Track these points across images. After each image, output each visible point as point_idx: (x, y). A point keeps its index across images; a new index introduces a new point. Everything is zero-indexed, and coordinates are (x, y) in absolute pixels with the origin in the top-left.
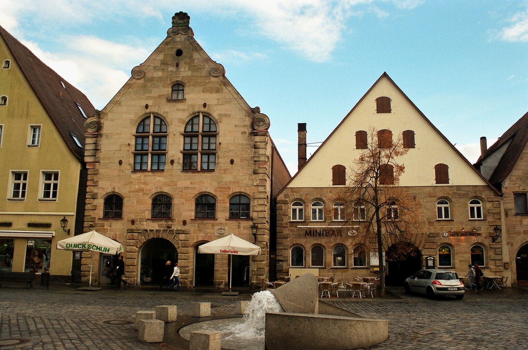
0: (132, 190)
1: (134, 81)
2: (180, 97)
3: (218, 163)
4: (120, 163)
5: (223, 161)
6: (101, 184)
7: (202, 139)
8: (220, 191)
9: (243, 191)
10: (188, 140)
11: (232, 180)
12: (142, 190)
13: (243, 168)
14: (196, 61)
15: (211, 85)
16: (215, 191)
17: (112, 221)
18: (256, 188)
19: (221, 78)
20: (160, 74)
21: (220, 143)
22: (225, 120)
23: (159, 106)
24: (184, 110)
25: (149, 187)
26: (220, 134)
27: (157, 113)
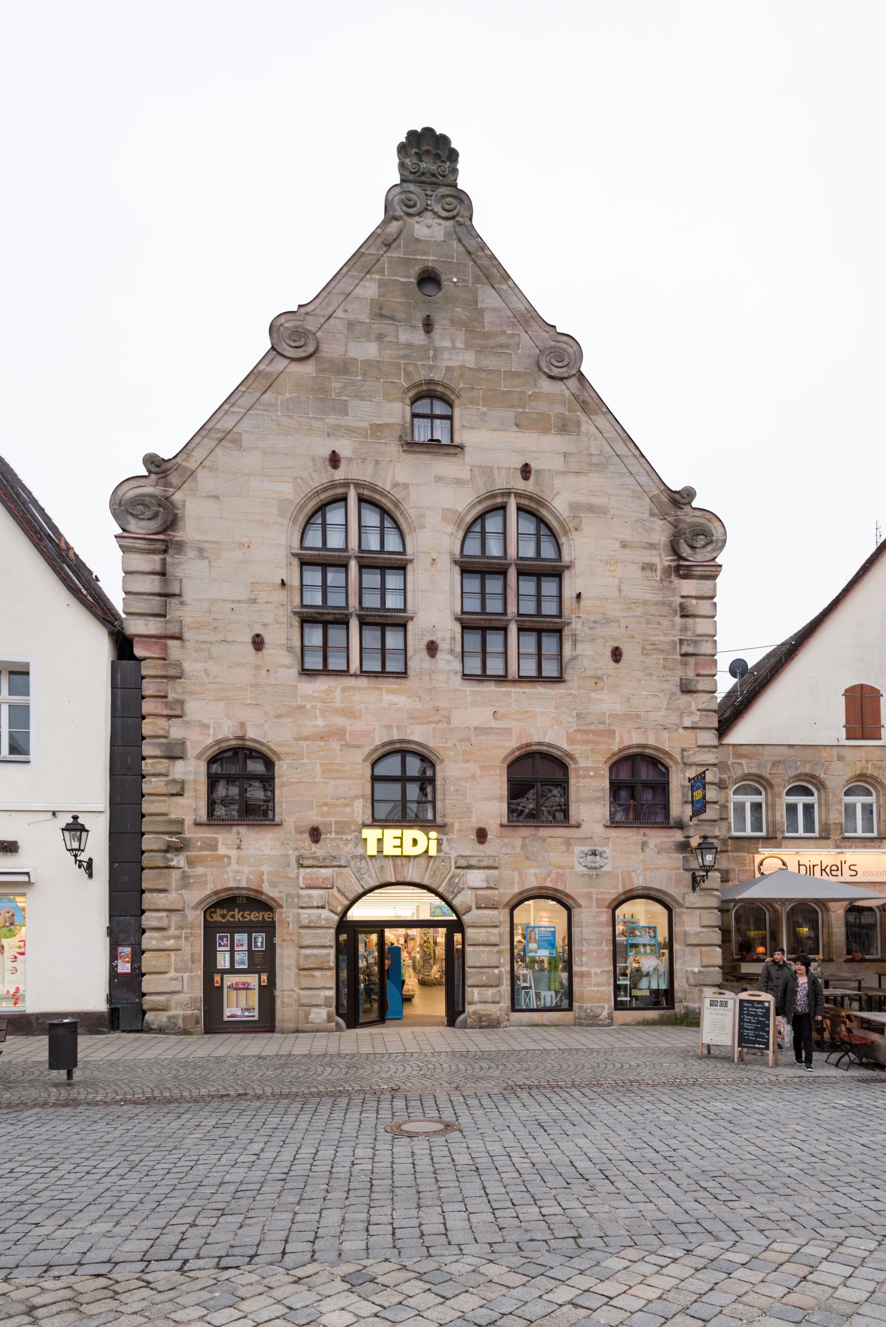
0: (306, 732)
1: (280, 364)
2: (441, 433)
3: (574, 658)
4: (258, 643)
5: (586, 652)
6: (194, 709)
7: (518, 600)
8: (586, 742)
9: (651, 742)
10: (473, 584)
11: (619, 709)
12: (340, 734)
13: (650, 675)
14: (488, 318)
15: (542, 406)
16: (571, 741)
17: (243, 830)
18: (688, 733)
19: (573, 383)
20: (369, 350)
21: (579, 596)
22: (590, 526)
23: (377, 462)
24: (459, 482)
25: (359, 726)
26: (579, 566)
27: (373, 488)
